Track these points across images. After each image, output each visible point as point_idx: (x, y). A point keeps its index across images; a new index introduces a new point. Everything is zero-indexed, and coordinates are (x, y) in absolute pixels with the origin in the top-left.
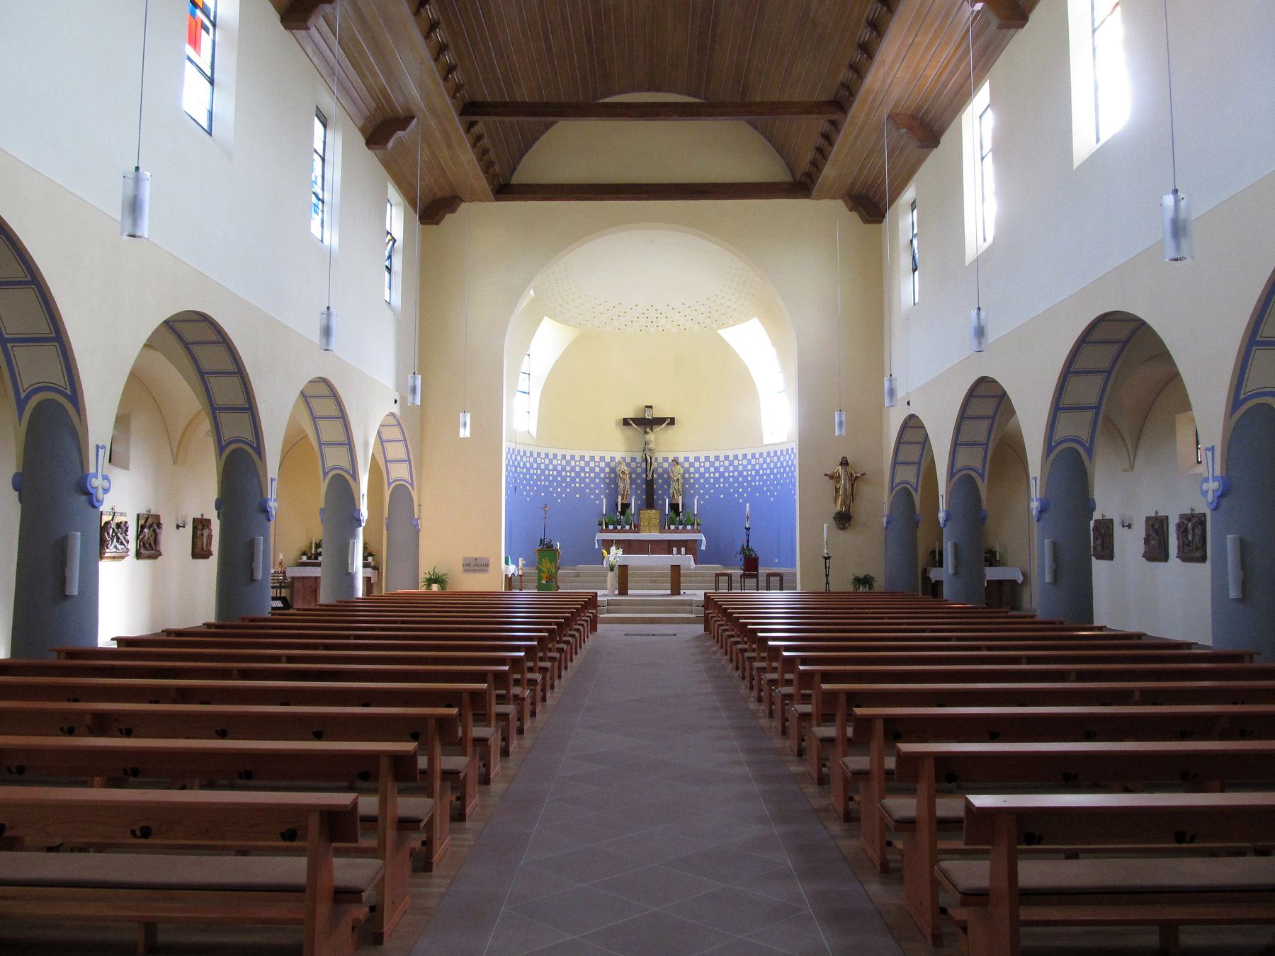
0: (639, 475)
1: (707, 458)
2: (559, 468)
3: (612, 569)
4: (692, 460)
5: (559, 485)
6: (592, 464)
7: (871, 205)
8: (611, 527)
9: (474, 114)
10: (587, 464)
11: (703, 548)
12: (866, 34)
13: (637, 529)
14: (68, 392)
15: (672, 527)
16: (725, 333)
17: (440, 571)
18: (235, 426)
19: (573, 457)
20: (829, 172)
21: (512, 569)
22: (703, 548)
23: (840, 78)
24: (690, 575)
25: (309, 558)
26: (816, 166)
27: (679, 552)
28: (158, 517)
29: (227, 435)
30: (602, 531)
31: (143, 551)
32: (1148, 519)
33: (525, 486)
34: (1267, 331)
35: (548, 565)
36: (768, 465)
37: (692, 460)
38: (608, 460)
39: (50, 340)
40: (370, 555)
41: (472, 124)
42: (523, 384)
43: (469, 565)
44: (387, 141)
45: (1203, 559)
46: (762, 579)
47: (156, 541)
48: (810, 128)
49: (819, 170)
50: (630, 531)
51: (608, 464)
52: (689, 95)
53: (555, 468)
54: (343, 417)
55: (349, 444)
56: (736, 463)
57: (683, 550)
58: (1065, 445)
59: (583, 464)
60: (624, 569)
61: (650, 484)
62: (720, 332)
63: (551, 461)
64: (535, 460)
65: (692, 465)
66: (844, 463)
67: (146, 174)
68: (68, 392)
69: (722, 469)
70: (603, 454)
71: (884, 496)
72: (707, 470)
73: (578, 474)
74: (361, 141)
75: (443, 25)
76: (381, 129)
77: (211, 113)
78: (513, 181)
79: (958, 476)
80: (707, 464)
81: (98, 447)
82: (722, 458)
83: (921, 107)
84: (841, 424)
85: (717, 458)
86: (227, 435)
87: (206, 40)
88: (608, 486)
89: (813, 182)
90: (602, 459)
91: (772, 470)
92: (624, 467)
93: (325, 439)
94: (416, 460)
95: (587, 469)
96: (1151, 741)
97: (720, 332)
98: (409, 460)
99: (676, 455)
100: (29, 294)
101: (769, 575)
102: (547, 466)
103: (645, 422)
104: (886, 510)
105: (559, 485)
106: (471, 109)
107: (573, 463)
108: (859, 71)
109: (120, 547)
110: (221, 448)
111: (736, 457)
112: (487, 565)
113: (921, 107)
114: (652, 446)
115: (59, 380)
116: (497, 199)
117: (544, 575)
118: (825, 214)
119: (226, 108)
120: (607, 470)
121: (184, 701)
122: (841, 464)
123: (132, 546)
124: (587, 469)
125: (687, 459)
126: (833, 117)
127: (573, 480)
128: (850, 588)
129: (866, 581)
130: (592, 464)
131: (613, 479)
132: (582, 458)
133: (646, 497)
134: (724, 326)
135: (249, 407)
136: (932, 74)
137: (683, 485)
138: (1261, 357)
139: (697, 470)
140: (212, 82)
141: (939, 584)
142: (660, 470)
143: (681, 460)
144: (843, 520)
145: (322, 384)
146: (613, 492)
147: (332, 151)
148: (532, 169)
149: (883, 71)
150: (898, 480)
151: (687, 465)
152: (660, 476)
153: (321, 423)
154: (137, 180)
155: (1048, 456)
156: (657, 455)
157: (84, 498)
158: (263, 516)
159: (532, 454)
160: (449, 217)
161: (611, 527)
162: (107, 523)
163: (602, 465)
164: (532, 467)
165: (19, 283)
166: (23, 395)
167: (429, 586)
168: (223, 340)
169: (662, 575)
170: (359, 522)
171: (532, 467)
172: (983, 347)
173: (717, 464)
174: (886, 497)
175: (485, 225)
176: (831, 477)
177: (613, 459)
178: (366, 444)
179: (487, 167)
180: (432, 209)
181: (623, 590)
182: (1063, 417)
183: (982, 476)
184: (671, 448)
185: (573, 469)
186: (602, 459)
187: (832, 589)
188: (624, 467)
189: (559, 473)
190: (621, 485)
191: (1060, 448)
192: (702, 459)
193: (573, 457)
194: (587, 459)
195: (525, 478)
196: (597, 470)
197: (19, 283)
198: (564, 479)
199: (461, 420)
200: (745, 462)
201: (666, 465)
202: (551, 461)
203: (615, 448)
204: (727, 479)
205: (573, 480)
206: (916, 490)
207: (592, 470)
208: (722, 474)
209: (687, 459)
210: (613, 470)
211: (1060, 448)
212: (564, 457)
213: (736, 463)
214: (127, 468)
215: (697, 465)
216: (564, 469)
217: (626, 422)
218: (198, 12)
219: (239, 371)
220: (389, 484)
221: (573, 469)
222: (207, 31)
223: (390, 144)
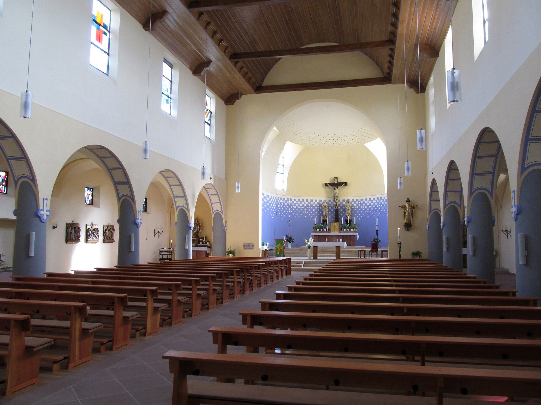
1: (362, 200)
2: (297, 205)
3: (309, 248)
4: (355, 200)
5: (297, 212)
6: (312, 203)
7: (419, 85)
8: (318, 230)
9: (236, 58)
10: (309, 203)
11: (358, 239)
12: (394, 9)
13: (329, 230)
14: (31, 178)
16: (366, 145)
17: (232, 249)
18: (123, 190)
19: (295, 200)
20: (395, 72)
21: (266, 248)
22: (358, 239)
23: (389, 30)
24: (344, 251)
25: (203, 243)
26: (390, 69)
27: (339, 241)
28: (113, 226)
29: (121, 194)
30: (314, 232)
31: (106, 240)
32: (67, 224)
33: (281, 213)
34: (534, 133)
35: (280, 246)
36: (381, 203)
37: (355, 200)
38: (318, 201)
39: (10, 159)
40: (208, 242)
41: (237, 63)
42: (280, 169)
43: (246, 246)
44: (201, 72)
46: (379, 252)
47: (112, 236)
48: (384, 51)
49: (392, 71)
50: (326, 232)
51: (318, 203)
52: (337, 43)
53: (288, 205)
54: (181, 185)
55: (185, 196)
56: (374, 201)
57: (341, 240)
58: (479, 191)
59: (299, 203)
60: (315, 248)
61: (337, 211)
62: (365, 145)
63: (293, 202)
64: (286, 202)
66: (408, 201)
67: (30, 93)
68: (31, 178)
69: (368, 204)
70: (366, 198)
71: (427, 216)
72: (362, 205)
73: (305, 207)
74: (191, 73)
75: (212, 23)
76: (198, 67)
77: (108, 67)
78: (263, 85)
79: (448, 206)
80: (362, 202)
81: (44, 199)
82: (368, 200)
83: (428, 40)
84: (400, 183)
85: (366, 200)
86: (121, 194)
87: (105, 38)
89: (391, 76)
90: (316, 201)
91: (383, 205)
92: (325, 204)
93: (175, 194)
94: (225, 202)
95: (309, 205)
97: (365, 145)
98: (220, 203)
99: (348, 198)
100: (12, 141)
101: (382, 251)
102: (284, 204)
103: (335, 185)
104: (428, 222)
105: (297, 212)
106: (234, 57)
107: (303, 203)
108: (395, 25)
109: (94, 238)
110: (119, 199)
111: (374, 199)
112: (253, 246)
114: (337, 195)
115: (28, 174)
116: (257, 93)
117: (278, 251)
118: (400, 91)
119: (114, 64)
120: (318, 205)
121: (20, 298)
122: (407, 201)
123: (101, 237)
124: (309, 205)
125: (353, 200)
126: (391, 47)
127: (288, 210)
128: (410, 257)
129: (418, 254)
130: (312, 203)
131: (321, 209)
132: (299, 200)
133: (335, 216)
135: (128, 182)
136: (428, 23)
137: (351, 212)
138: (533, 147)
139: (357, 205)
140: (108, 54)
141: (465, 256)
142: (341, 205)
143: (350, 201)
144: (408, 226)
145: (170, 172)
147: (170, 76)
148: (270, 80)
149: (405, 24)
150: (432, 208)
151: (353, 203)
152: (341, 207)
153: (173, 188)
154: (27, 96)
155: (470, 197)
156: (339, 199)
157: (38, 219)
158: (135, 226)
159: (284, 199)
160: (237, 102)
161: (318, 230)
162: (89, 229)
163: (316, 203)
164: (284, 204)
165: (7, 137)
166: (16, 180)
167: (228, 255)
168: (113, 156)
169: (333, 251)
170: (190, 228)
171: (284, 204)
172: (457, 98)
173: (366, 202)
174: (428, 216)
175: (252, 104)
176: (402, 207)
177: (321, 201)
178: (194, 196)
179: (249, 80)
180: (229, 98)
181: (315, 257)
182: (476, 178)
184: (346, 195)
185: (303, 205)
187: (402, 257)
188: (325, 204)
189: (297, 207)
191: (476, 193)
192: (359, 200)
193: (303, 200)
194: (309, 201)
195: (281, 209)
196: (314, 205)
197: (7, 137)
198: (299, 209)
199: (402, 186)
200: (370, 202)
201: (344, 203)
202: (293, 202)
203: (321, 196)
204: (370, 209)
205: (303, 210)
206: (222, 213)
207: (312, 205)
208: (368, 207)
209: (353, 200)
210: (321, 205)
211: (476, 193)
212: (291, 200)
213: (374, 201)
214: (99, 207)
216: (299, 205)
217: (326, 185)
218: (101, 28)
219: (122, 168)
220: (213, 213)
221: (303, 205)
222: (106, 34)
223: (202, 74)
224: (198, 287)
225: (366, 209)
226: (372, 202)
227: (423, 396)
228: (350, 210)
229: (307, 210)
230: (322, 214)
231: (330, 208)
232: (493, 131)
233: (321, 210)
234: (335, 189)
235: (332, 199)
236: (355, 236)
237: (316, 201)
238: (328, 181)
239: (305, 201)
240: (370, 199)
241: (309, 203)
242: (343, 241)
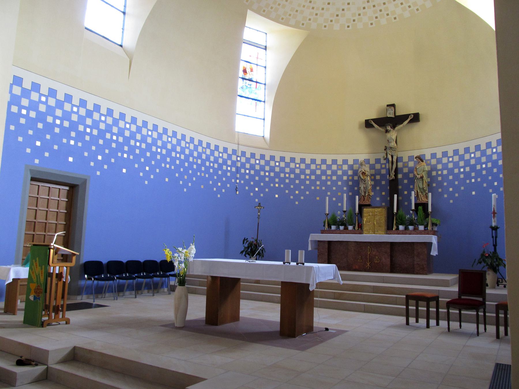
0: (383, 177)
1: (456, 152)
4: (439, 155)
5: (297, 187)
6: (313, 167)
8: (333, 227)
10: (308, 166)
11: (434, 252)
13: (360, 229)
15: (401, 227)
30: (323, 232)
37: (439, 155)
50: (353, 232)
51: (351, 167)
65: (439, 161)
80: (456, 158)
92: (366, 168)
96: (10, 340)
103: (390, 121)
105: (257, 184)
114: (393, 144)
120: (350, 172)
131: (355, 182)
132: (303, 161)
142: (406, 170)
143: (428, 157)
151: (434, 162)
152: (406, 176)
161: (333, 227)
163: (345, 167)
173: (467, 157)
188: (366, 168)
190: (362, 186)
192: (450, 154)
194: (308, 161)
196: (340, 173)
198: (262, 179)
201: (411, 164)
203: (357, 150)
205: (272, 180)
207: (313, 172)
209: (433, 156)
215: (445, 160)
217: (368, 124)
221: (292, 171)
225: (467, 175)
226: (483, 153)
228: (426, 179)
230: (358, 193)
231: (378, 177)
233: (356, 183)
234: (387, 131)
235: (381, 156)
236: (429, 245)
237: (345, 162)
238: (373, 115)
239: (298, 161)
240: (478, 148)
241: (230, 157)
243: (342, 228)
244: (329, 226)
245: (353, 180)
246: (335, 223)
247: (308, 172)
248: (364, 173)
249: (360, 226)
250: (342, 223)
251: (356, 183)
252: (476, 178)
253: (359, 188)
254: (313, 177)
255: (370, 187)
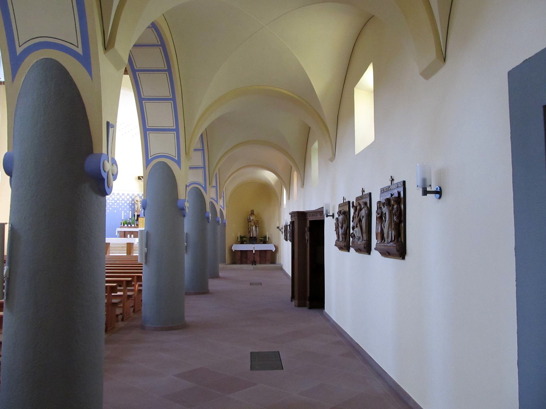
10: (121, 197)
27: (130, 237)
30: (121, 227)
38: (131, 195)
45: (310, 221)
50: (134, 227)
51: (131, 197)
57: (132, 236)
83: (303, 184)
88: (131, 207)
92: (138, 198)
95: (121, 199)
113: (303, 184)
120: (131, 200)
130: (123, 197)
131: (133, 205)
134: (80, 54)
146: (133, 210)
161: (126, 225)
163: (128, 197)
169: (122, 247)
177: (133, 195)
183: (178, 162)
186: (128, 195)
188: (138, 198)
190: (136, 206)
196: (126, 199)
207: (123, 200)
210: (133, 200)
224: (129, 288)
227: (311, 307)
229: (118, 204)
232: (4, 168)
233: (134, 205)
241: (121, 197)
242: (134, 237)
243: (129, 225)
244: (124, 225)
245: (132, 203)
246: (127, 223)
247: (121, 199)
248: (137, 201)
249: (137, 225)
250: (128, 224)
251: (134, 205)
252: (117, 205)
253: (135, 207)
254: (113, 201)
255: (139, 207)
